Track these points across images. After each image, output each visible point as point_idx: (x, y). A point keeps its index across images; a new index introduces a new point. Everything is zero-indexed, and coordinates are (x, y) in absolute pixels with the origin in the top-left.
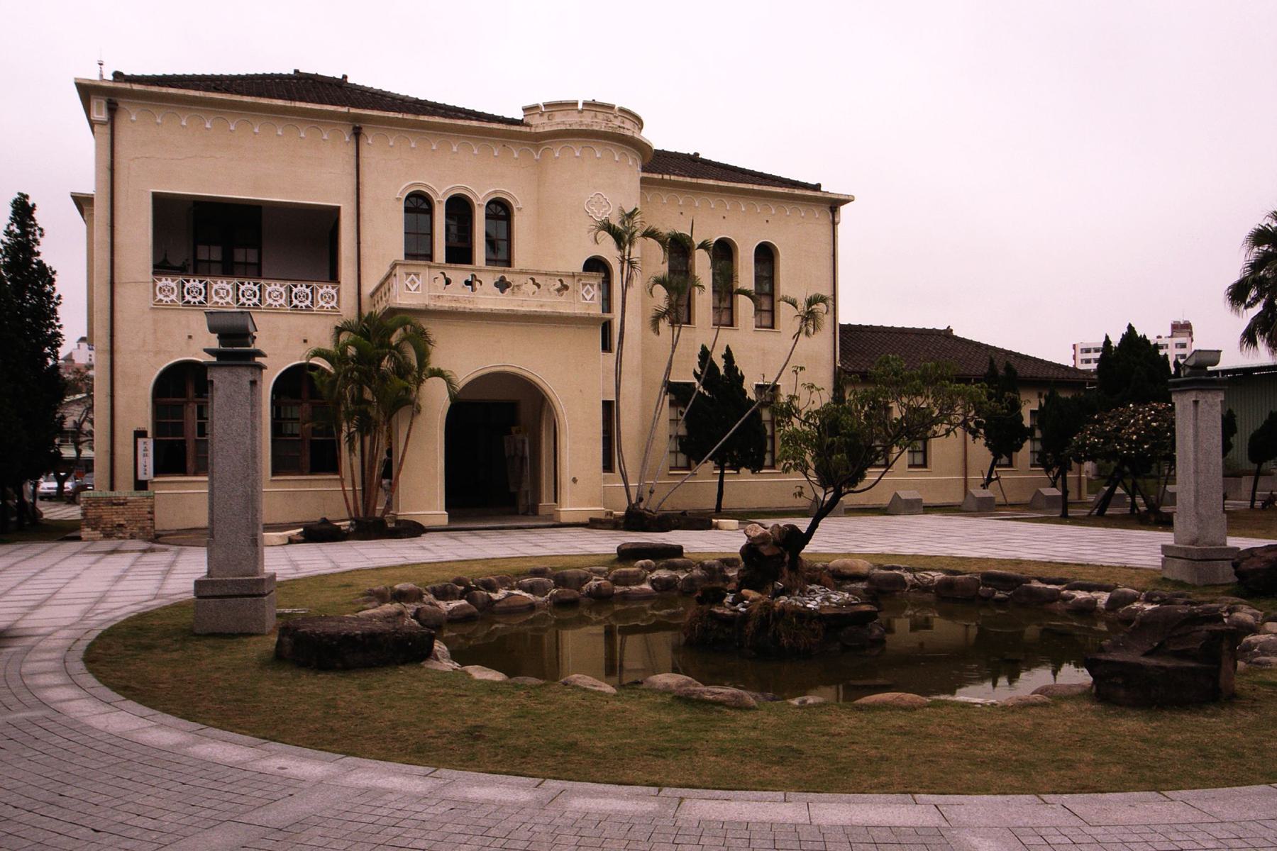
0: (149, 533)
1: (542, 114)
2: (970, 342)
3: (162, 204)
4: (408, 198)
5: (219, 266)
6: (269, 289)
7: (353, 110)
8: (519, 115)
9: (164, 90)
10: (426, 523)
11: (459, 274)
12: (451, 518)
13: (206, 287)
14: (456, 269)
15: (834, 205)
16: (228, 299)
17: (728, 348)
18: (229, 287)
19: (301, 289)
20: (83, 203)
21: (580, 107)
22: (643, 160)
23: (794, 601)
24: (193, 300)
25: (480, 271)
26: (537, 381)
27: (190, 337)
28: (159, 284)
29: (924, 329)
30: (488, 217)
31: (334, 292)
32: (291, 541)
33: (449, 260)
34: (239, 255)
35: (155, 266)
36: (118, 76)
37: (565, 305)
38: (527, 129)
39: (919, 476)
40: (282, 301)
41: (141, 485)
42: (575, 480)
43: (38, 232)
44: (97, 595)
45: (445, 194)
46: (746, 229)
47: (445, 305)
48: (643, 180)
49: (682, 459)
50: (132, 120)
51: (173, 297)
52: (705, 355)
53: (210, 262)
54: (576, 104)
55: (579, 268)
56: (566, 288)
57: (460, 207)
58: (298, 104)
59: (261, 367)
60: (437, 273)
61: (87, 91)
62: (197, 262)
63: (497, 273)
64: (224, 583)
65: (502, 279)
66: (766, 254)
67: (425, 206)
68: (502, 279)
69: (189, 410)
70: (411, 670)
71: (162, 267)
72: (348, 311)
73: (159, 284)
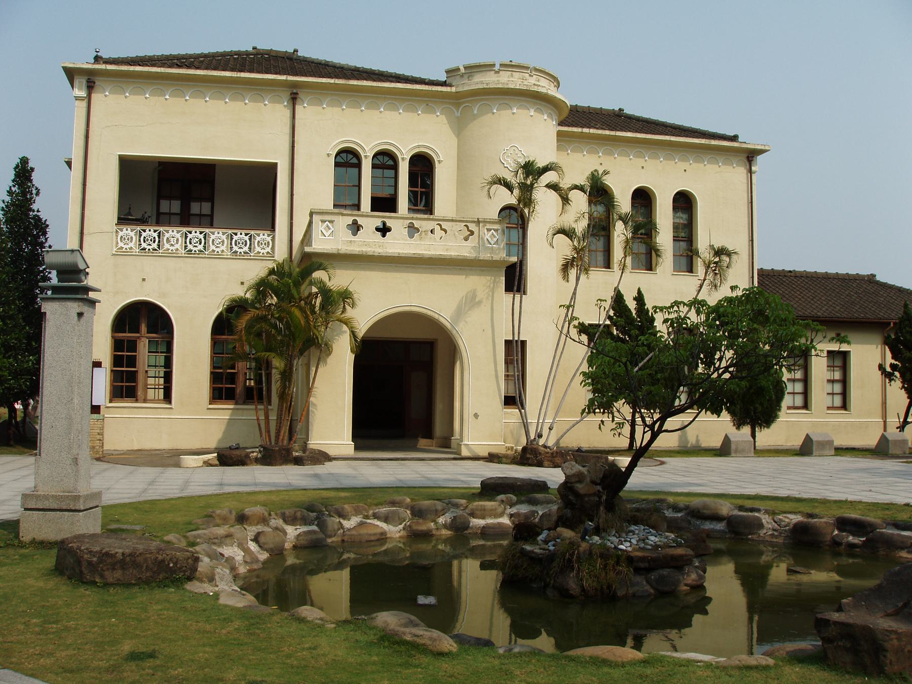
0: (97, 452)
1: (462, 76)
2: (892, 287)
5: (178, 218)
7: (290, 78)
8: (443, 78)
9: (132, 68)
10: (332, 452)
12: (357, 448)
15: (750, 156)
16: (178, 246)
17: (639, 292)
19: (241, 236)
21: (463, 70)
22: (560, 114)
23: (612, 541)
24: (239, 250)
26: (436, 316)
27: (144, 280)
28: (121, 234)
30: (374, 166)
31: (269, 239)
33: (373, 209)
34: (195, 208)
35: (119, 219)
39: (840, 417)
41: (96, 409)
42: (476, 416)
43: (34, 192)
45: (372, 149)
46: (665, 177)
47: (355, 249)
48: (560, 134)
51: (131, 245)
52: (618, 299)
53: (170, 214)
54: (494, 65)
56: (472, 233)
57: (385, 160)
58: (243, 75)
59: (92, 303)
62: (159, 214)
64: (46, 497)
65: (355, 223)
66: (684, 202)
67: (391, 163)
68: (355, 223)
69: (142, 344)
70: (172, 592)
71: (124, 219)
72: (281, 254)
73: (121, 234)
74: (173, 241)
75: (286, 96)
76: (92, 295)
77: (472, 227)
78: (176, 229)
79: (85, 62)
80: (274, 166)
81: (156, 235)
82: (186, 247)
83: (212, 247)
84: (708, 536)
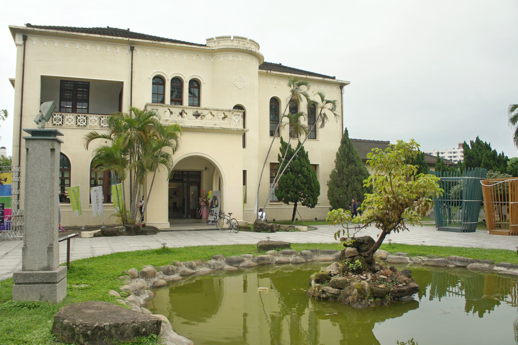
1: (215, 42)
3: (44, 79)
4: (154, 78)
6: (91, 118)
7: (130, 39)
10: (159, 227)
11: (177, 110)
12: (171, 224)
13: (63, 118)
14: (175, 107)
15: (342, 86)
16: (72, 123)
18: (73, 118)
20: (12, 82)
21: (232, 38)
22: (260, 63)
24: (57, 123)
25: (187, 108)
29: (378, 141)
32: (95, 235)
36: (29, 25)
37: (225, 124)
38: (208, 48)
40: (96, 124)
44: (6, 257)
45: (171, 76)
49: (275, 198)
50: (33, 43)
54: (230, 37)
55: (231, 108)
57: (177, 82)
60: (166, 109)
61: (14, 31)
63: (194, 110)
74: (70, 120)
75: (128, 48)
76: (59, 137)
77: (227, 113)
78: (71, 115)
79: (21, 24)
80: (122, 83)
81: (61, 117)
82: (77, 124)
83: (91, 124)
84: (315, 252)
